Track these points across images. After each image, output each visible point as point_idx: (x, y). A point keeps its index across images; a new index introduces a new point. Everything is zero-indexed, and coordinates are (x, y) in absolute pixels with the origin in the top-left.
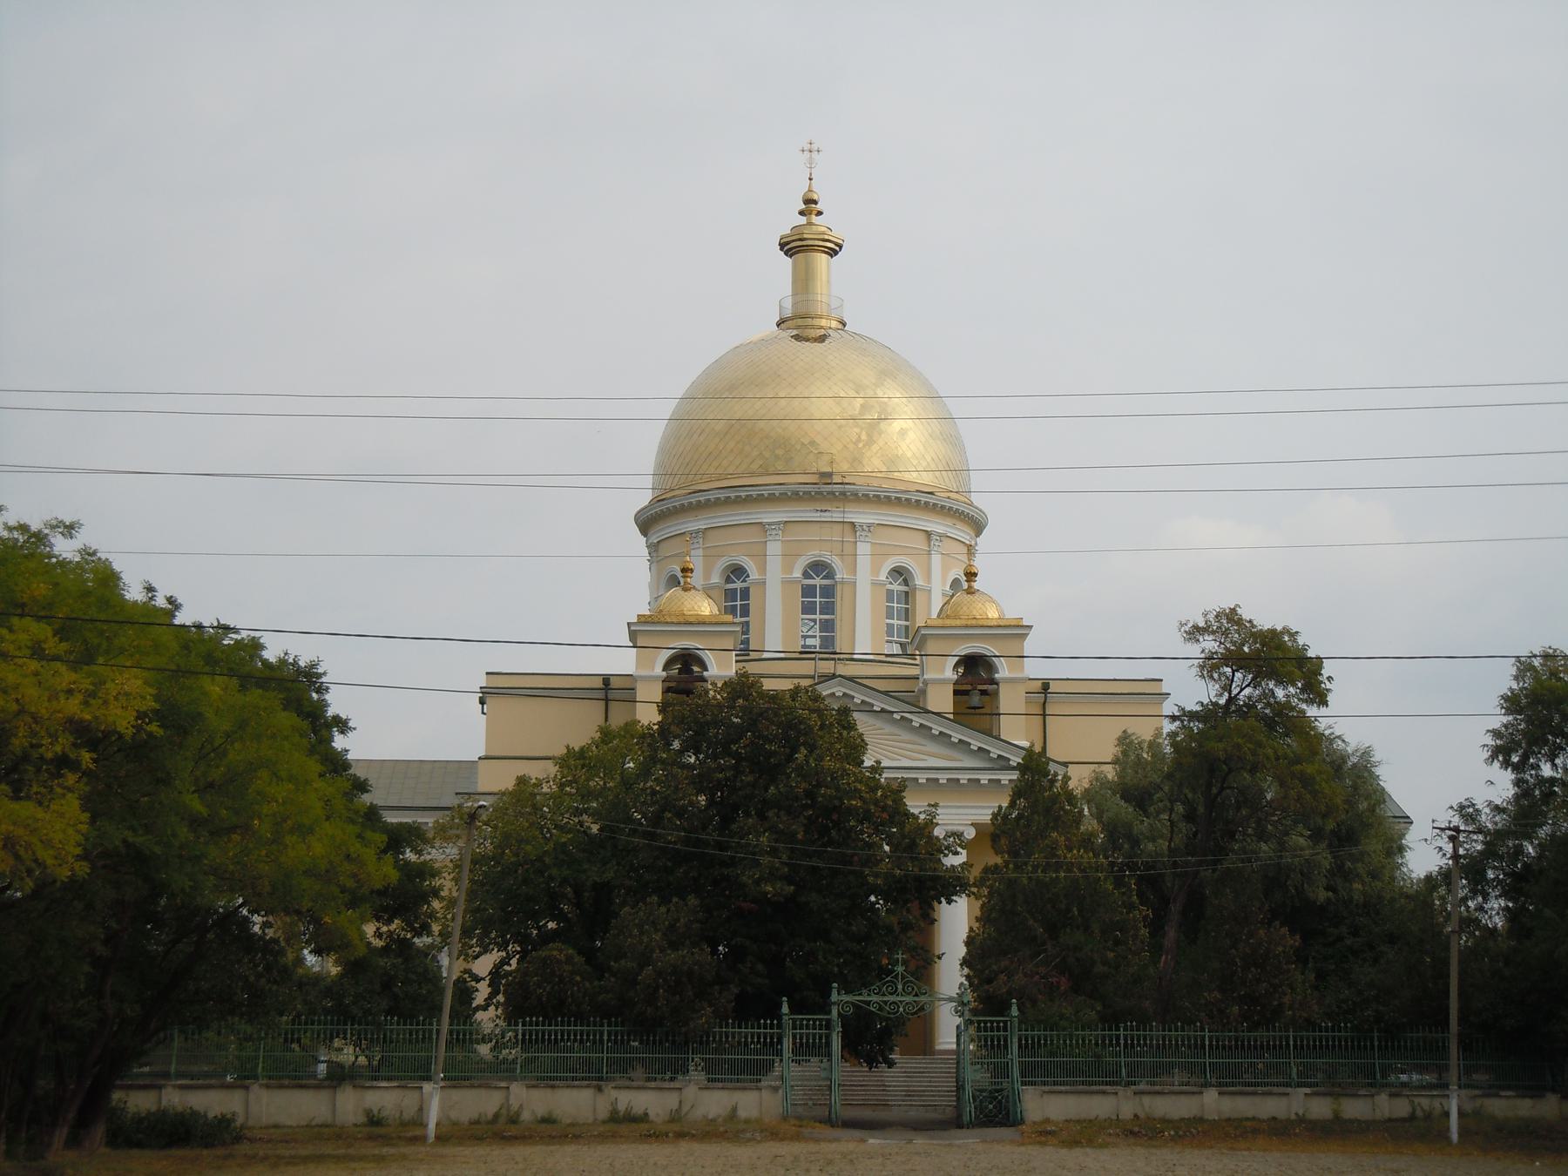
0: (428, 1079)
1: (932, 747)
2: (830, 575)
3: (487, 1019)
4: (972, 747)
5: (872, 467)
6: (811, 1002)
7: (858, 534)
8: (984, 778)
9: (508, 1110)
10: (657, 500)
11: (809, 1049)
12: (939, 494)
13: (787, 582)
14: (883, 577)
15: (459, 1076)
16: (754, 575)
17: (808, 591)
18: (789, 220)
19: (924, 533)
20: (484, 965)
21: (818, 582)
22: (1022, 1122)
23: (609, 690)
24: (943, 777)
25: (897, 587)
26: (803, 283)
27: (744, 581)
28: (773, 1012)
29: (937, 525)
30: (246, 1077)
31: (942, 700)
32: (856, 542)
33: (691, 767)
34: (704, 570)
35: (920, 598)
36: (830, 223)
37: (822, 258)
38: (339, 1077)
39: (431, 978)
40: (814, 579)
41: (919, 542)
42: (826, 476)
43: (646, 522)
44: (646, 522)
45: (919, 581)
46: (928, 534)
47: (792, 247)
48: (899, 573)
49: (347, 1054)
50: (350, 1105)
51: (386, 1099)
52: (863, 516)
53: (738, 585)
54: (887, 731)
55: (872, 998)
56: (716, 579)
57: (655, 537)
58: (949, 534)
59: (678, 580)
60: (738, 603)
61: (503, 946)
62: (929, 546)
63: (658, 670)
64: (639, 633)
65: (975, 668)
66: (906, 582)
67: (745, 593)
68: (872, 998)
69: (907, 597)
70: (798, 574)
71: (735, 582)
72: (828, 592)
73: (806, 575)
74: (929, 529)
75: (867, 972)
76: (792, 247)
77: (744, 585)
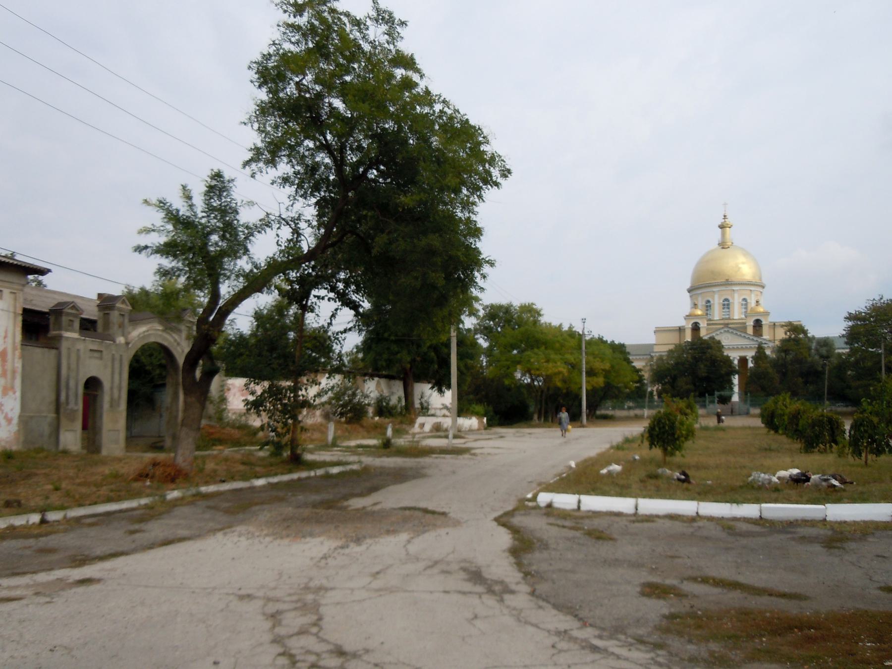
0: (645, 408)
1: (746, 340)
2: (729, 301)
3: (656, 397)
5: (737, 278)
6: (711, 394)
9: (354, 395)
10: (691, 287)
11: (712, 402)
12: (721, 326)
13: (719, 303)
14: (741, 300)
15: (650, 407)
16: (712, 302)
17: (724, 305)
18: (720, 221)
20: (655, 389)
21: (726, 303)
22: (459, 416)
23: (681, 330)
24: (748, 346)
25: (744, 303)
28: (704, 396)
29: (752, 288)
30: (614, 408)
31: (750, 331)
34: (701, 302)
37: (728, 229)
38: (630, 408)
39: (645, 391)
41: (748, 292)
42: (727, 280)
43: (689, 291)
44: (689, 291)
45: (749, 301)
47: (722, 227)
48: (744, 300)
49: (631, 404)
50: (632, 413)
51: (638, 412)
52: (735, 288)
53: (708, 304)
55: (722, 393)
56: (704, 303)
59: (695, 306)
61: (658, 384)
63: (690, 326)
64: (688, 317)
65: (758, 324)
67: (710, 306)
68: (722, 393)
69: (746, 305)
70: (721, 301)
72: (728, 305)
75: (722, 388)
76: (722, 227)
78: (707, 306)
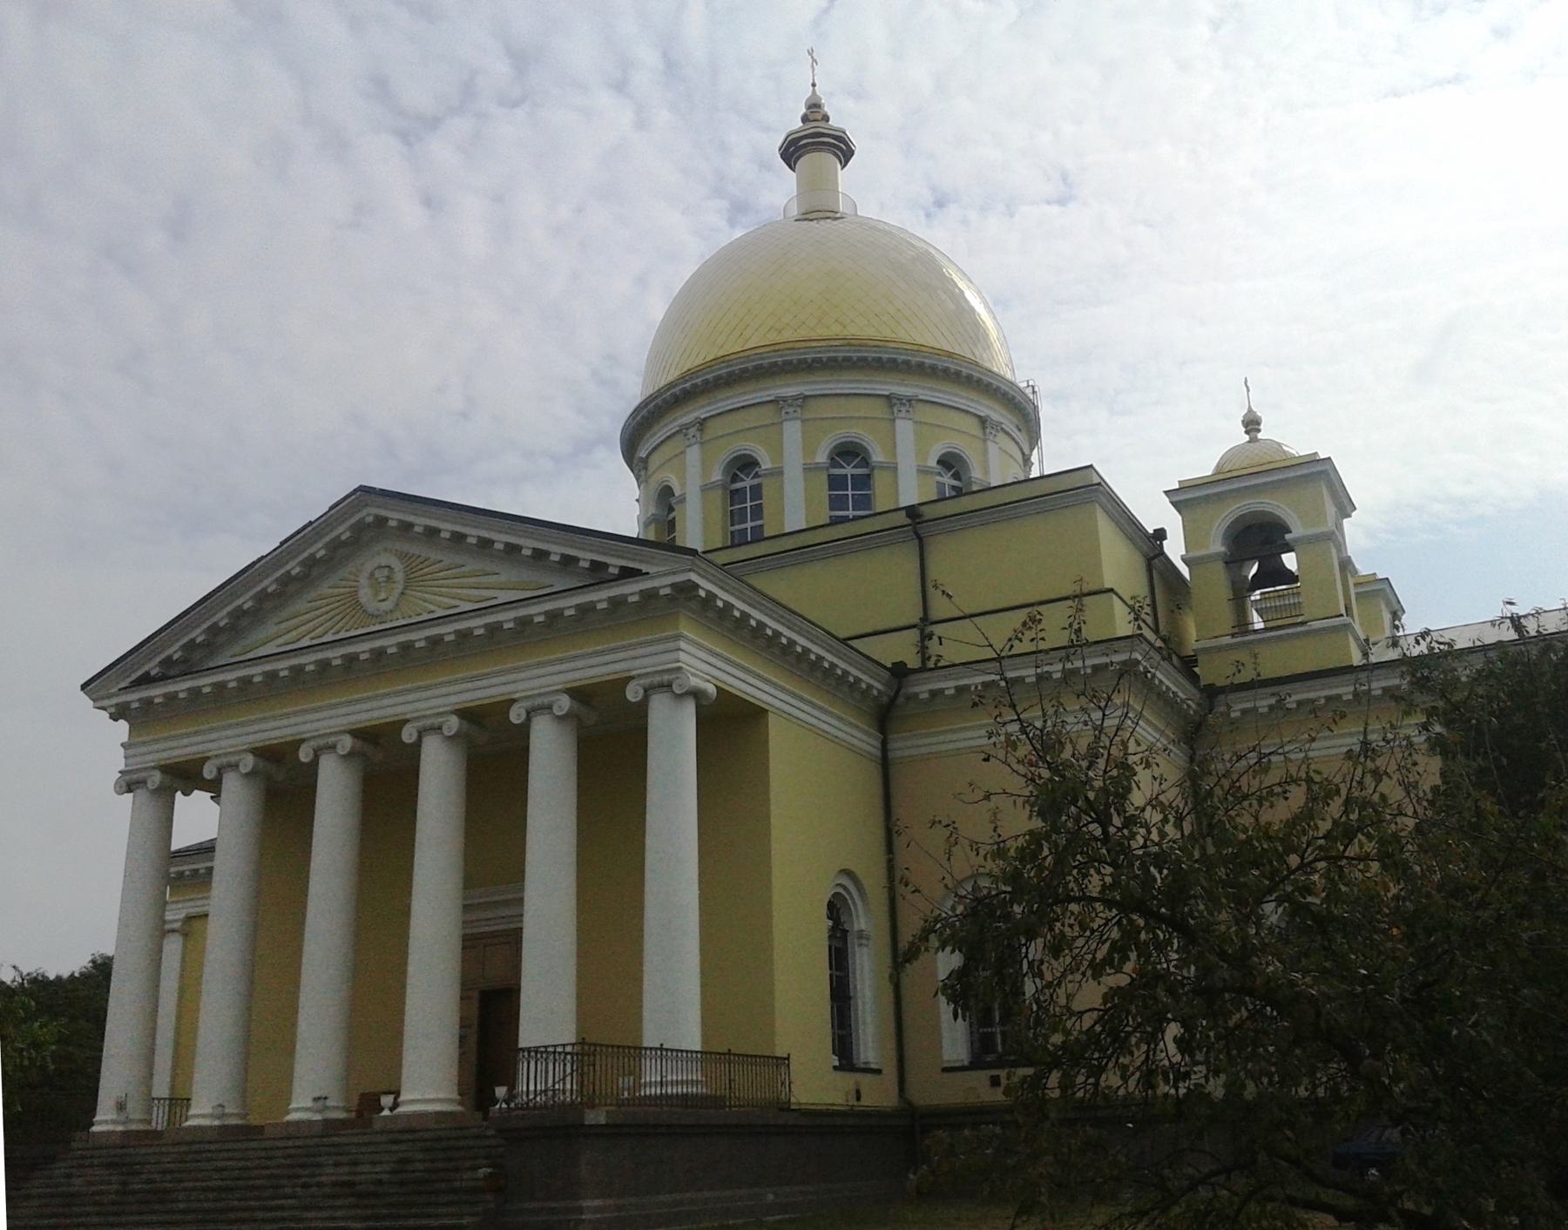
2: (866, 462)
4: (1345, 698)
7: (988, 431)
8: (568, 604)
13: (809, 469)
16: (766, 464)
17: (836, 482)
19: (881, 402)
21: (849, 471)
26: (806, 188)
27: (757, 476)
32: (894, 420)
33: (1533, 849)
35: (880, 481)
36: (841, 116)
40: (844, 467)
41: (972, 426)
46: (983, 421)
54: (503, 578)
57: (702, 411)
58: (921, 397)
60: (749, 504)
62: (985, 434)
66: (957, 476)
67: (757, 491)
70: (822, 457)
71: (743, 480)
73: (833, 463)
74: (982, 414)
76: (792, 151)
77: (756, 481)
78: (735, 496)
